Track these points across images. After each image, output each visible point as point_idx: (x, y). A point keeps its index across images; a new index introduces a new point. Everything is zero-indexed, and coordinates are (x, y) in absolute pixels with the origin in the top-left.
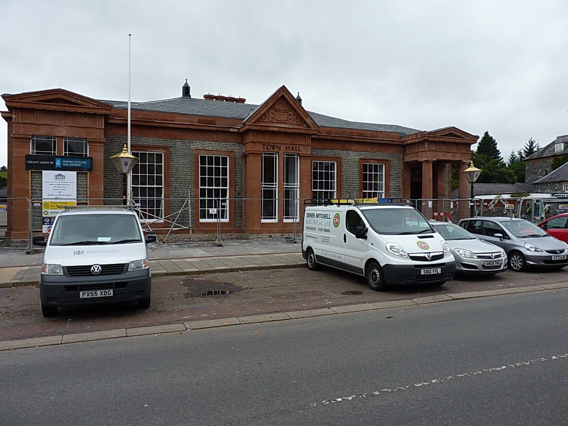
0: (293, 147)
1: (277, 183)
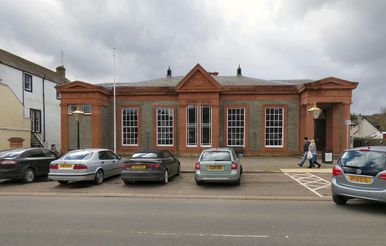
1: (211, 123)
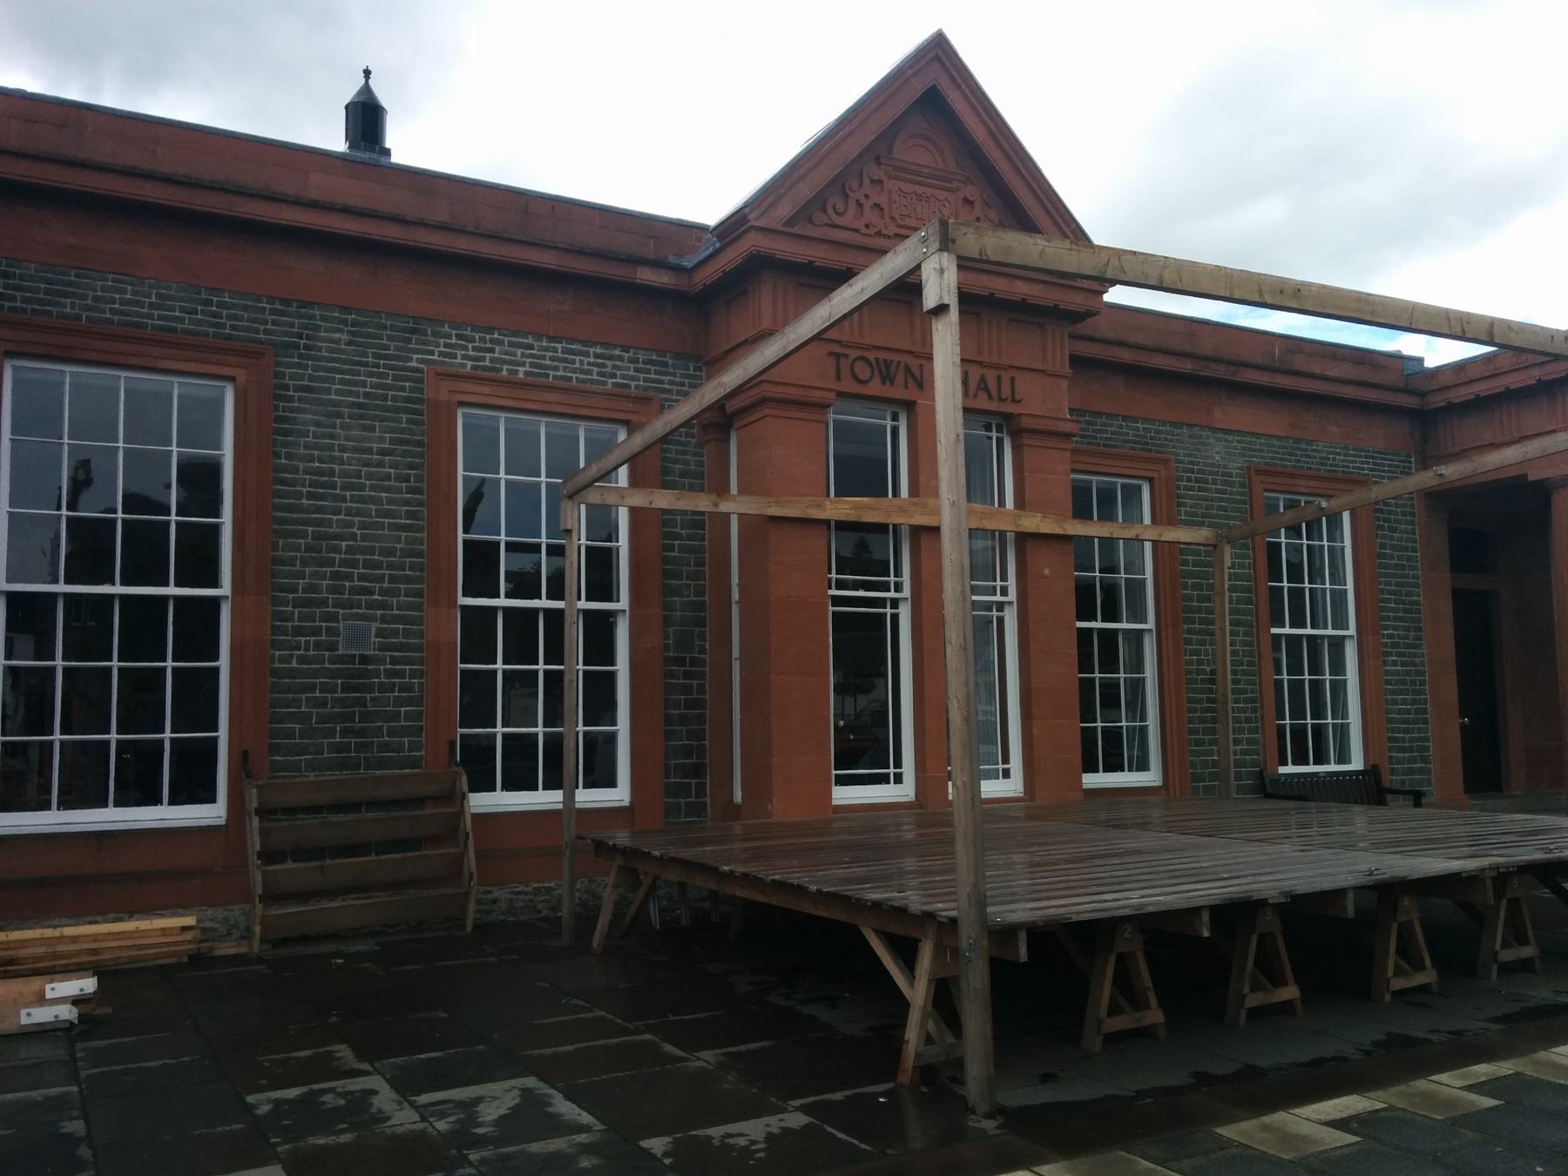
0: (983, 379)
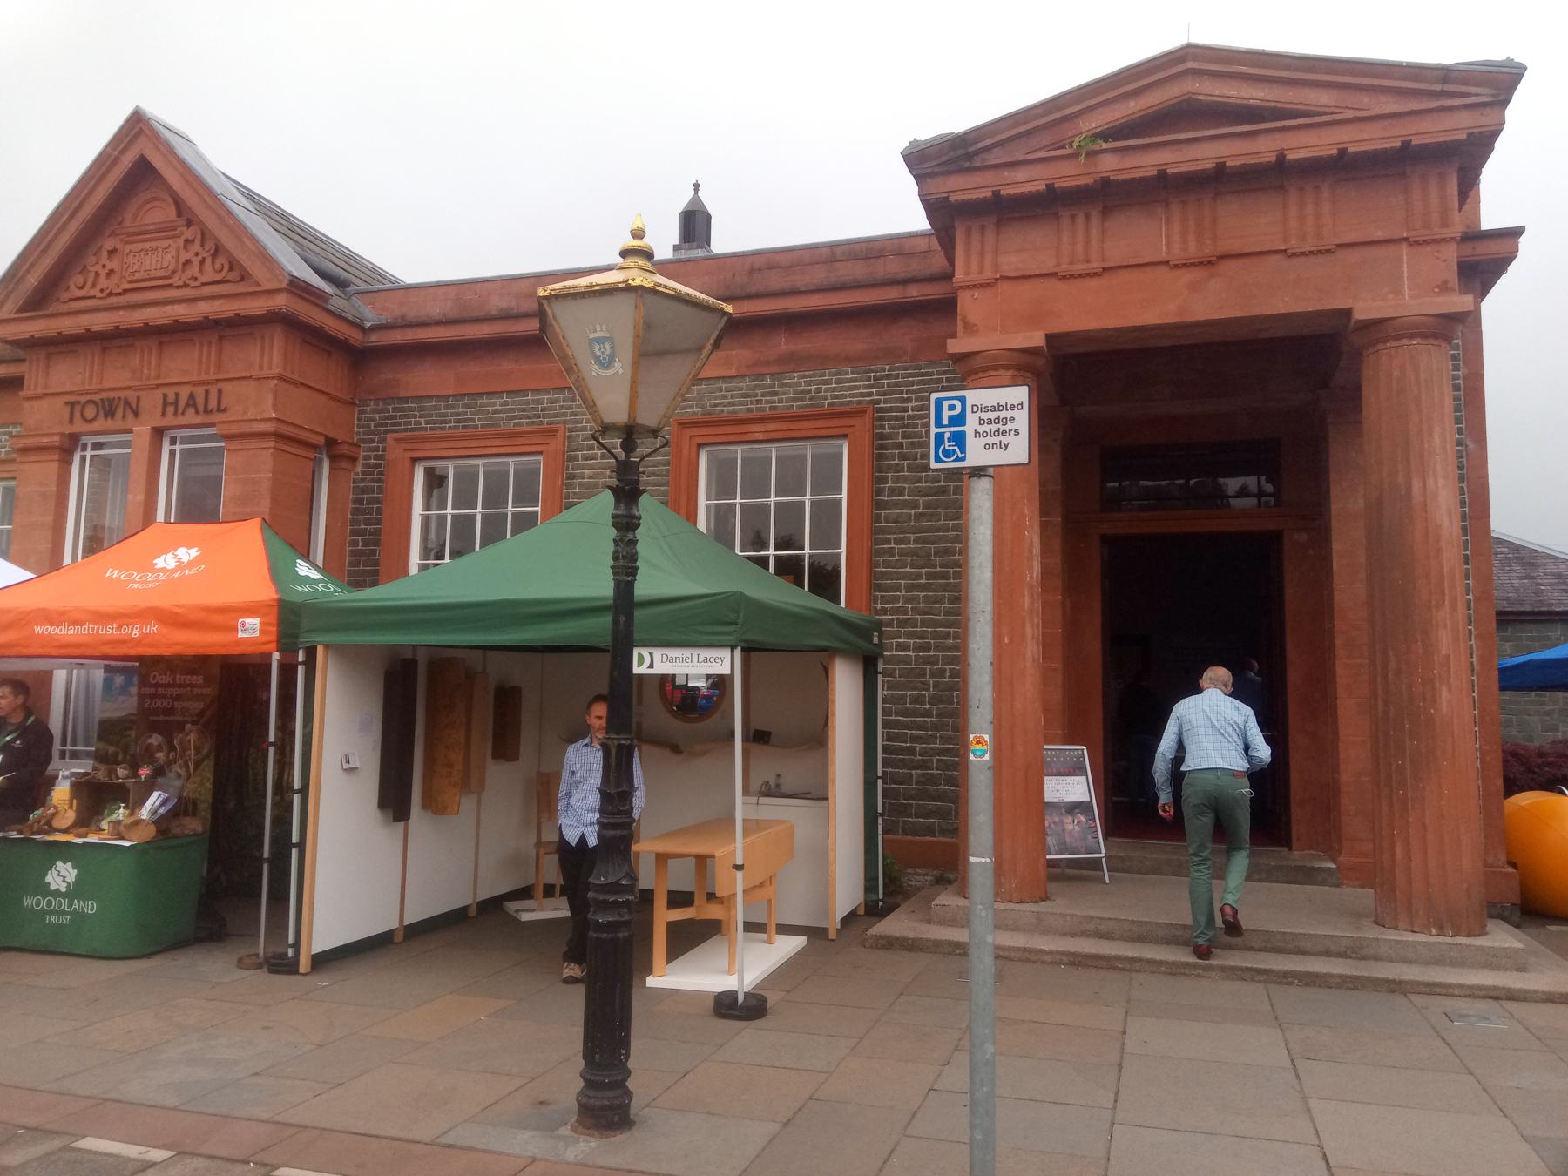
0: (192, 396)
